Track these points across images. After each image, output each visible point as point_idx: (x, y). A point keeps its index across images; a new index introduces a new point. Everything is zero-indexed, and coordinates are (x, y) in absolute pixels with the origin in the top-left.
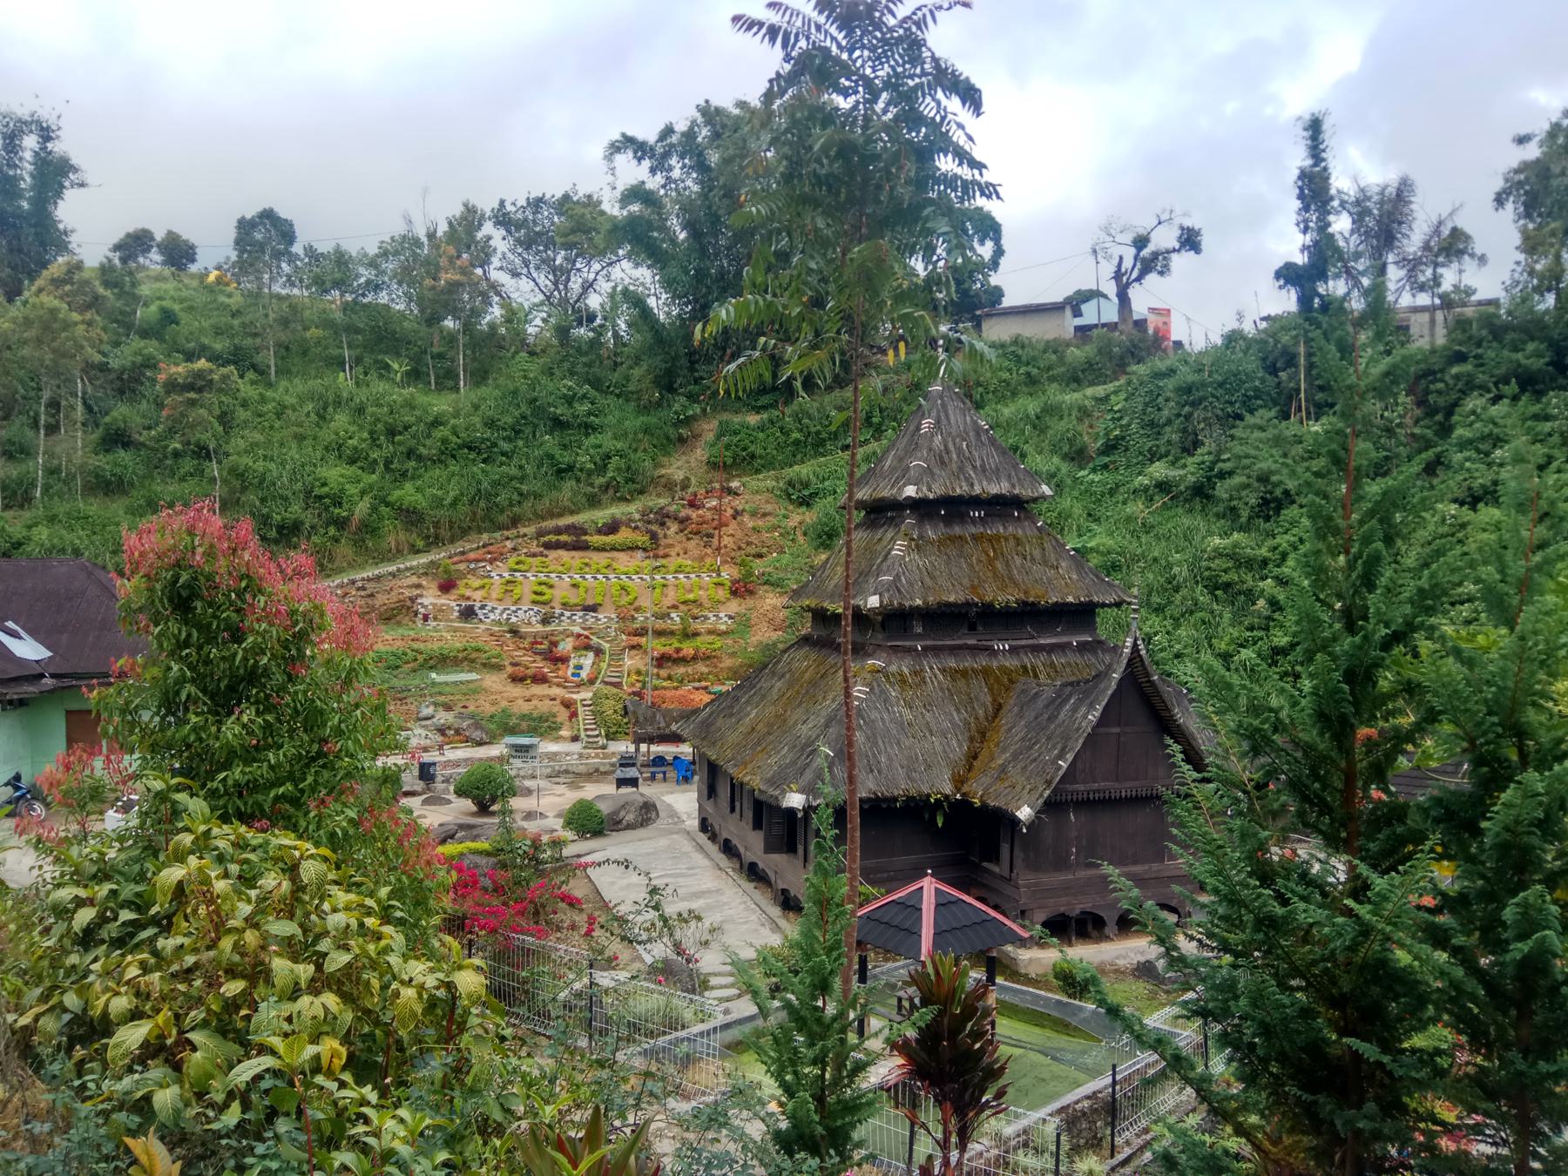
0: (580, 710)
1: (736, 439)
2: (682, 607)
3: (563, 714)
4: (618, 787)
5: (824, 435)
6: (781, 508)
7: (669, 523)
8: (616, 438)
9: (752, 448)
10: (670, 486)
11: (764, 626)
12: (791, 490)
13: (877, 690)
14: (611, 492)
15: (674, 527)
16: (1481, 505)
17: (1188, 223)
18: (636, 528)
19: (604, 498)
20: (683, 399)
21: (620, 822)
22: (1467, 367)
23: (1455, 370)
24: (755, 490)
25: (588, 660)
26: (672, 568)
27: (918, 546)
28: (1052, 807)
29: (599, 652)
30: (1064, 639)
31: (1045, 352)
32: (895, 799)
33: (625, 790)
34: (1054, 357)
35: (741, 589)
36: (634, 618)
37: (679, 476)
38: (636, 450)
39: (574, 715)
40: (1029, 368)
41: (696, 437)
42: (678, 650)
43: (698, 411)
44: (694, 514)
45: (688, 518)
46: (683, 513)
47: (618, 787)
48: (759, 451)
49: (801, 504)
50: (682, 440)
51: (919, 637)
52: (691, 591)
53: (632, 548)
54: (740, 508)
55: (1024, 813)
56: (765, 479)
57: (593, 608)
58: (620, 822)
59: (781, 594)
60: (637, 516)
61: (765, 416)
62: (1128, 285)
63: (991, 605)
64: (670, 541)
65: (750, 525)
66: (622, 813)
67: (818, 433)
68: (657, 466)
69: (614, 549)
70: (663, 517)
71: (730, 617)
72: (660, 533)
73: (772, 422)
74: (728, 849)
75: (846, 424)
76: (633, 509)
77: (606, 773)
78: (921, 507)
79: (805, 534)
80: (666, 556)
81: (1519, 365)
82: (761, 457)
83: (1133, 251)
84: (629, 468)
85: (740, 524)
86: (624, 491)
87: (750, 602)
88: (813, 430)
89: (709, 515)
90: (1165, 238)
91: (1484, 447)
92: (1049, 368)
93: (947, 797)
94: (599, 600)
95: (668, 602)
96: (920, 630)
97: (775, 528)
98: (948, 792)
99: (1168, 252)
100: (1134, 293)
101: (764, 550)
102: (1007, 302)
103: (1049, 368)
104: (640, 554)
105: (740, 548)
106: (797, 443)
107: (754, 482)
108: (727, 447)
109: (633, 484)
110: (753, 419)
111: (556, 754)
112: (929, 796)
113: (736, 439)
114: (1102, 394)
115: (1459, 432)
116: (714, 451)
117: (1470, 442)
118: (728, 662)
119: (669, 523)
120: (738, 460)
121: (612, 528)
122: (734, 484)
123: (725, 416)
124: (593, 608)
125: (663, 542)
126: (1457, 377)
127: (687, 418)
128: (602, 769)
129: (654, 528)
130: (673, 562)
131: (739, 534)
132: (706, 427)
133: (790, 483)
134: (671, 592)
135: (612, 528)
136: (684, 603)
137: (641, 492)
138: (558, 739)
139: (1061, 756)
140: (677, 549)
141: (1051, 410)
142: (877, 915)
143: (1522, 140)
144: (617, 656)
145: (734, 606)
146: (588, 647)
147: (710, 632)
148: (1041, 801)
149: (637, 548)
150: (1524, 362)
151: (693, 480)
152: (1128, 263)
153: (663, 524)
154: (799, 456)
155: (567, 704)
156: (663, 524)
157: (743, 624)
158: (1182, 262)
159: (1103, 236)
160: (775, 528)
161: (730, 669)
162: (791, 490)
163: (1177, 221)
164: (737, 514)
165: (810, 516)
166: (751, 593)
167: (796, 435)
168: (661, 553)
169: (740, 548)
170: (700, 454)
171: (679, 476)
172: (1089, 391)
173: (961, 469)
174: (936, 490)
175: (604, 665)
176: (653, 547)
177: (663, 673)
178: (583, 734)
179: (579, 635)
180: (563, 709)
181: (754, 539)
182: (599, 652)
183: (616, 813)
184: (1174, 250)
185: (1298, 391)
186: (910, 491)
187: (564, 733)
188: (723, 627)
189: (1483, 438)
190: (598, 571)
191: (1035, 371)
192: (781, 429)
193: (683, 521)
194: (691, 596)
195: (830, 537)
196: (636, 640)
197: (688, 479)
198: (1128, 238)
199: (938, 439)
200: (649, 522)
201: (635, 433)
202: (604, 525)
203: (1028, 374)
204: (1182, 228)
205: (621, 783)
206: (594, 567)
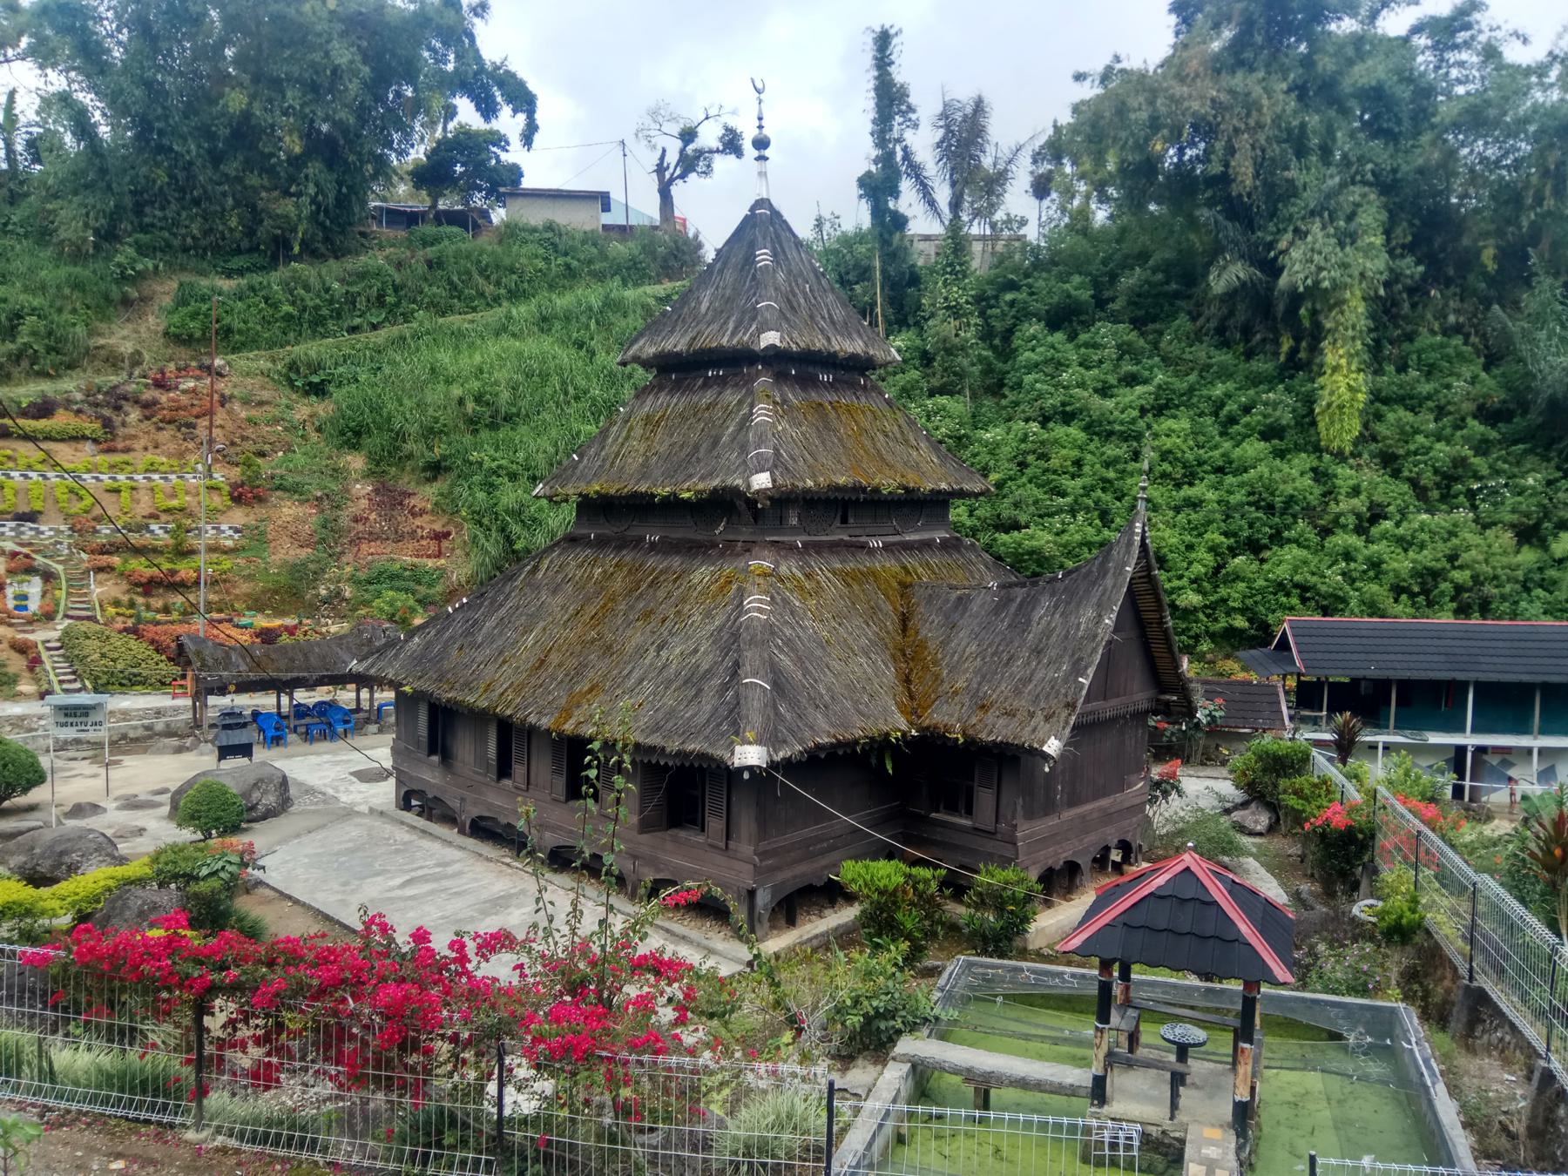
0: (45, 655)
1: (204, 307)
2: (164, 517)
3: (17, 663)
4: (222, 757)
5: (325, 312)
6: (284, 396)
7: (127, 407)
8: (26, 289)
9: (227, 320)
10: (113, 361)
11: (286, 543)
12: (293, 376)
13: (778, 598)
14: (25, 364)
15: (134, 415)
16: (1051, 425)
17: (731, 124)
18: (79, 411)
19: (15, 372)
20: (131, 251)
21: (253, 808)
22: (1021, 296)
23: (1009, 297)
24: (245, 372)
25: (34, 587)
26: (141, 467)
27: (783, 408)
28: (1084, 730)
29: (48, 576)
30: (926, 536)
31: (584, 242)
32: (856, 742)
33: (232, 763)
34: (594, 250)
35: (241, 496)
36: (96, 531)
37: (127, 348)
38: (60, 310)
39: (37, 661)
40: (568, 259)
41: (145, 300)
42: (173, 572)
43: (150, 266)
44: (163, 398)
45: (155, 402)
46: (147, 395)
47: (222, 757)
48: (237, 324)
49: (307, 394)
50: (126, 302)
51: (794, 530)
52: (174, 496)
53: (77, 438)
54: (227, 392)
55: (1053, 747)
56: (257, 358)
57: (31, 517)
58: (253, 808)
59: (302, 502)
60: (79, 396)
61: (243, 282)
62: (672, 180)
63: (876, 490)
64: (133, 431)
65: (243, 415)
66: (256, 795)
67: (317, 308)
68: (92, 333)
69: (49, 438)
70: (118, 400)
71: (237, 531)
72: (117, 420)
73: (252, 288)
74: (485, 830)
75: (351, 300)
76: (70, 385)
77: (137, 740)
78: (776, 360)
79: (319, 430)
80: (127, 450)
81: (1069, 296)
82: (240, 332)
83: (679, 144)
84: (50, 333)
85: (230, 412)
86: (46, 362)
87: (260, 511)
88: (310, 304)
89: (184, 399)
90: (709, 136)
91: (1049, 370)
92: (590, 262)
93: (904, 734)
94: (37, 506)
95: (144, 508)
96: (794, 521)
97: (276, 421)
98: (904, 727)
99: (711, 152)
100: (677, 190)
101: (267, 447)
102: (527, 183)
103: (590, 262)
104: (89, 447)
105: (233, 444)
106: (288, 318)
107: (242, 361)
108: (194, 316)
109: (60, 355)
110: (226, 284)
111: (22, 718)
112: (887, 734)
113: (204, 307)
114: (662, 294)
115: (1026, 356)
116: (176, 319)
117: (1036, 365)
118: (244, 588)
119: (127, 407)
120: (201, 337)
121: (44, 409)
122: (218, 362)
123: (187, 278)
124: (31, 517)
125: (121, 431)
126: (1012, 304)
127: (139, 273)
128: (132, 735)
129: (107, 412)
130: (142, 459)
131: (230, 426)
132: (159, 288)
133: (293, 366)
134: (145, 498)
135: (44, 409)
136: (168, 511)
137: (71, 366)
138: (16, 697)
139: (1078, 669)
140: (143, 442)
141: (611, 305)
142: (1139, 919)
143: (1079, 77)
144: (78, 583)
145: (239, 516)
146: (30, 570)
147: (212, 549)
148: (1068, 730)
149: (85, 438)
150: (1073, 293)
151: (147, 356)
152: (672, 158)
153: (118, 408)
154: (292, 335)
155: (21, 648)
156: (118, 408)
157: (256, 539)
158: (723, 164)
159: (648, 121)
160: (276, 421)
161: (248, 595)
162: (293, 376)
163: (723, 119)
164: (224, 400)
165: (323, 409)
166: (260, 500)
167: (287, 308)
168: (120, 445)
169: (233, 444)
170: (154, 322)
171: (127, 348)
172: (649, 289)
173: (812, 317)
174: (800, 341)
175: (61, 594)
176: (108, 439)
177: (157, 603)
178: (57, 687)
179: (14, 555)
180: (15, 656)
181: (249, 432)
182: (48, 576)
183: (246, 795)
184: (718, 151)
185: (873, 305)
186: (770, 338)
187: (25, 687)
188: (229, 543)
189: (1046, 362)
190: (30, 467)
191: (575, 263)
192: (266, 299)
193: (148, 407)
194: (175, 503)
195: (358, 434)
196: (105, 560)
197: (139, 353)
198: (675, 129)
199: (781, 276)
200: (97, 405)
201: (59, 287)
202: (31, 405)
203: (568, 266)
204: (727, 129)
205: (225, 752)
206: (22, 461)
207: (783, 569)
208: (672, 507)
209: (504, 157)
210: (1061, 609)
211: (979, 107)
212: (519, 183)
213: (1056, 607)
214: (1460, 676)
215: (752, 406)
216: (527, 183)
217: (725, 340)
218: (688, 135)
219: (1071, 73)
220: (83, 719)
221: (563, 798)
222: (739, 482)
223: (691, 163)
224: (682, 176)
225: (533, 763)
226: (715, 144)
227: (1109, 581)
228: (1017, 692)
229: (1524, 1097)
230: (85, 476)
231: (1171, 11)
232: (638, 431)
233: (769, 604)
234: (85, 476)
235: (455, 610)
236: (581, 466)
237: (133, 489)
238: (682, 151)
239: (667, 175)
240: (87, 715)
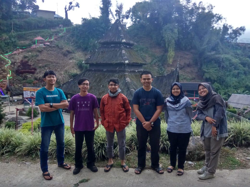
83: (69, 5)
99: (74, 6)
102: (40, 9)
152: (67, 7)
184: (75, 6)
186: (124, 41)
207: (129, 75)
208: (111, 65)
209: (35, 3)
210: (168, 80)
211: (121, 4)
212: (39, 9)
213: (167, 79)
214: (194, 90)
215: (122, 51)
216: (40, 9)
217: (116, 40)
218: (71, 3)
219: (215, 7)
220: (5, 99)
222: (123, 62)
223: (70, 8)
224: (69, 10)
226: (75, 5)
227: (174, 76)
228: (164, 91)
229: (40, 175)
232: (100, 53)
233: (130, 79)
235: (70, 81)
236: (91, 59)
238: (69, 6)
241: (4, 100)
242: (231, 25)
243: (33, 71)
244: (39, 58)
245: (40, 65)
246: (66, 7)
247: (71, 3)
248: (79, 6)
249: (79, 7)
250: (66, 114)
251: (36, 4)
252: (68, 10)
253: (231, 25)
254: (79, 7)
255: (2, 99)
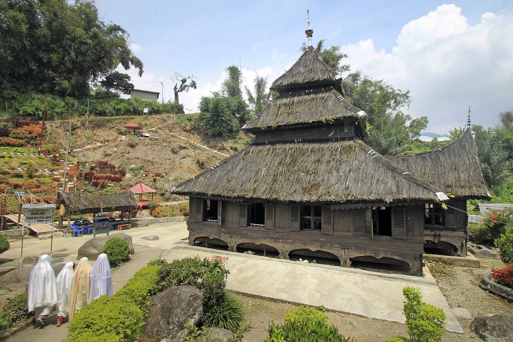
83: (182, 83)
102: (134, 88)
152: (178, 87)
204: (193, 81)
216: (134, 88)
218: (184, 81)
221: (298, 230)
223: (182, 89)
224: (181, 91)
225: (277, 218)
230: (18, 169)
231: (182, 105)
234: (18, 169)
237: (10, 157)
238: (182, 85)
239: (177, 90)
240: (43, 214)
241: (39, 216)
242: (34, 328)
243: (118, 178)
244: (131, 156)
245: (133, 166)
246: (176, 86)
247: (184, 81)
248: (196, 86)
249: (195, 87)
250: (235, 255)
251: (129, 82)
252: (178, 91)
253: (34, 328)
254: (195, 87)
255: (32, 214)
